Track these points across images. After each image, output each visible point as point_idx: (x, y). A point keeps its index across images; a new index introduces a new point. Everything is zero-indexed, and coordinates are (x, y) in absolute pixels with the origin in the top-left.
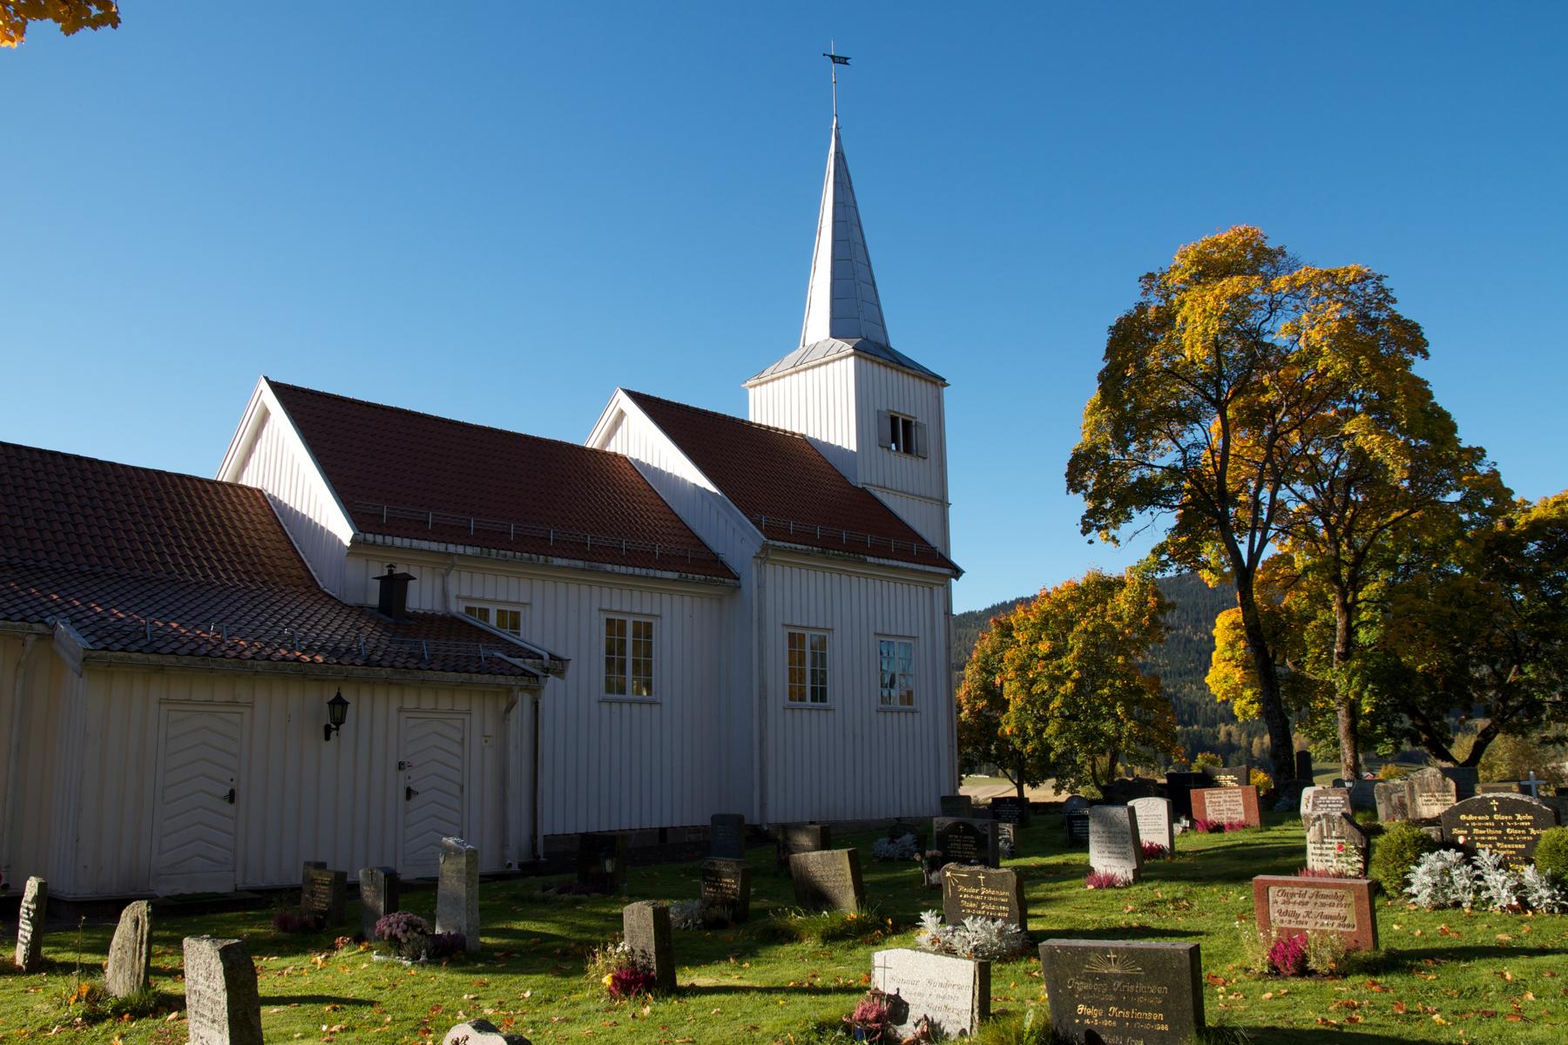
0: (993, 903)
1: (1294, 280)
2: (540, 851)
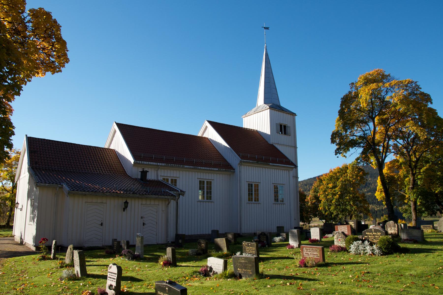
1: (390, 84)
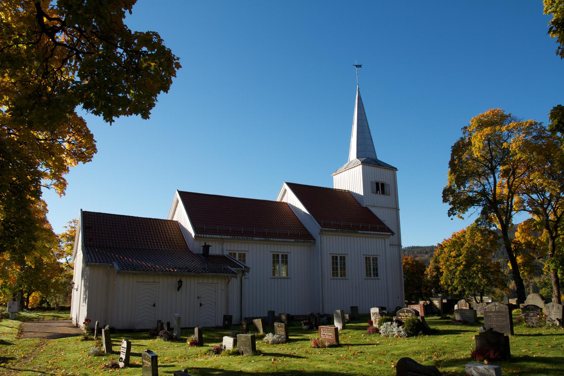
1: (508, 127)
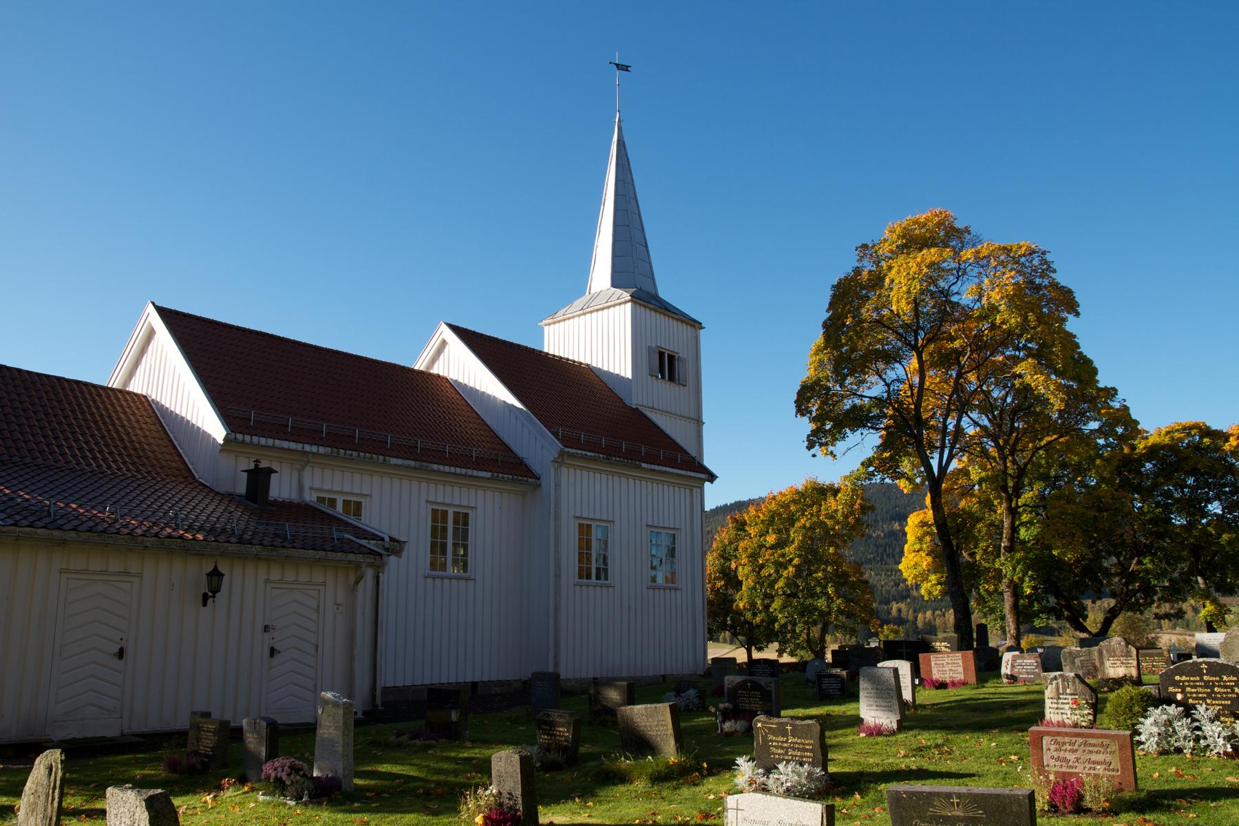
0: (799, 749)
1: (978, 252)
2: (379, 702)
